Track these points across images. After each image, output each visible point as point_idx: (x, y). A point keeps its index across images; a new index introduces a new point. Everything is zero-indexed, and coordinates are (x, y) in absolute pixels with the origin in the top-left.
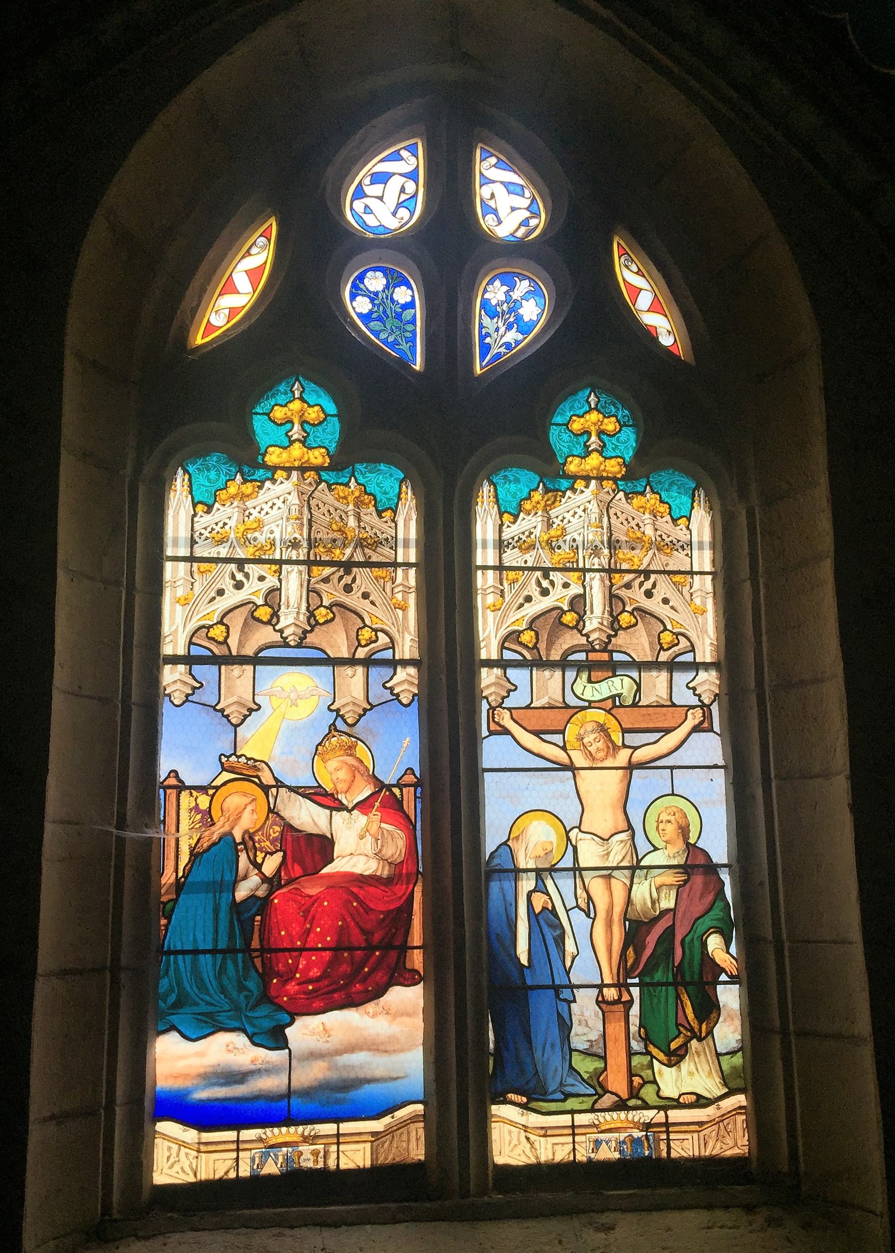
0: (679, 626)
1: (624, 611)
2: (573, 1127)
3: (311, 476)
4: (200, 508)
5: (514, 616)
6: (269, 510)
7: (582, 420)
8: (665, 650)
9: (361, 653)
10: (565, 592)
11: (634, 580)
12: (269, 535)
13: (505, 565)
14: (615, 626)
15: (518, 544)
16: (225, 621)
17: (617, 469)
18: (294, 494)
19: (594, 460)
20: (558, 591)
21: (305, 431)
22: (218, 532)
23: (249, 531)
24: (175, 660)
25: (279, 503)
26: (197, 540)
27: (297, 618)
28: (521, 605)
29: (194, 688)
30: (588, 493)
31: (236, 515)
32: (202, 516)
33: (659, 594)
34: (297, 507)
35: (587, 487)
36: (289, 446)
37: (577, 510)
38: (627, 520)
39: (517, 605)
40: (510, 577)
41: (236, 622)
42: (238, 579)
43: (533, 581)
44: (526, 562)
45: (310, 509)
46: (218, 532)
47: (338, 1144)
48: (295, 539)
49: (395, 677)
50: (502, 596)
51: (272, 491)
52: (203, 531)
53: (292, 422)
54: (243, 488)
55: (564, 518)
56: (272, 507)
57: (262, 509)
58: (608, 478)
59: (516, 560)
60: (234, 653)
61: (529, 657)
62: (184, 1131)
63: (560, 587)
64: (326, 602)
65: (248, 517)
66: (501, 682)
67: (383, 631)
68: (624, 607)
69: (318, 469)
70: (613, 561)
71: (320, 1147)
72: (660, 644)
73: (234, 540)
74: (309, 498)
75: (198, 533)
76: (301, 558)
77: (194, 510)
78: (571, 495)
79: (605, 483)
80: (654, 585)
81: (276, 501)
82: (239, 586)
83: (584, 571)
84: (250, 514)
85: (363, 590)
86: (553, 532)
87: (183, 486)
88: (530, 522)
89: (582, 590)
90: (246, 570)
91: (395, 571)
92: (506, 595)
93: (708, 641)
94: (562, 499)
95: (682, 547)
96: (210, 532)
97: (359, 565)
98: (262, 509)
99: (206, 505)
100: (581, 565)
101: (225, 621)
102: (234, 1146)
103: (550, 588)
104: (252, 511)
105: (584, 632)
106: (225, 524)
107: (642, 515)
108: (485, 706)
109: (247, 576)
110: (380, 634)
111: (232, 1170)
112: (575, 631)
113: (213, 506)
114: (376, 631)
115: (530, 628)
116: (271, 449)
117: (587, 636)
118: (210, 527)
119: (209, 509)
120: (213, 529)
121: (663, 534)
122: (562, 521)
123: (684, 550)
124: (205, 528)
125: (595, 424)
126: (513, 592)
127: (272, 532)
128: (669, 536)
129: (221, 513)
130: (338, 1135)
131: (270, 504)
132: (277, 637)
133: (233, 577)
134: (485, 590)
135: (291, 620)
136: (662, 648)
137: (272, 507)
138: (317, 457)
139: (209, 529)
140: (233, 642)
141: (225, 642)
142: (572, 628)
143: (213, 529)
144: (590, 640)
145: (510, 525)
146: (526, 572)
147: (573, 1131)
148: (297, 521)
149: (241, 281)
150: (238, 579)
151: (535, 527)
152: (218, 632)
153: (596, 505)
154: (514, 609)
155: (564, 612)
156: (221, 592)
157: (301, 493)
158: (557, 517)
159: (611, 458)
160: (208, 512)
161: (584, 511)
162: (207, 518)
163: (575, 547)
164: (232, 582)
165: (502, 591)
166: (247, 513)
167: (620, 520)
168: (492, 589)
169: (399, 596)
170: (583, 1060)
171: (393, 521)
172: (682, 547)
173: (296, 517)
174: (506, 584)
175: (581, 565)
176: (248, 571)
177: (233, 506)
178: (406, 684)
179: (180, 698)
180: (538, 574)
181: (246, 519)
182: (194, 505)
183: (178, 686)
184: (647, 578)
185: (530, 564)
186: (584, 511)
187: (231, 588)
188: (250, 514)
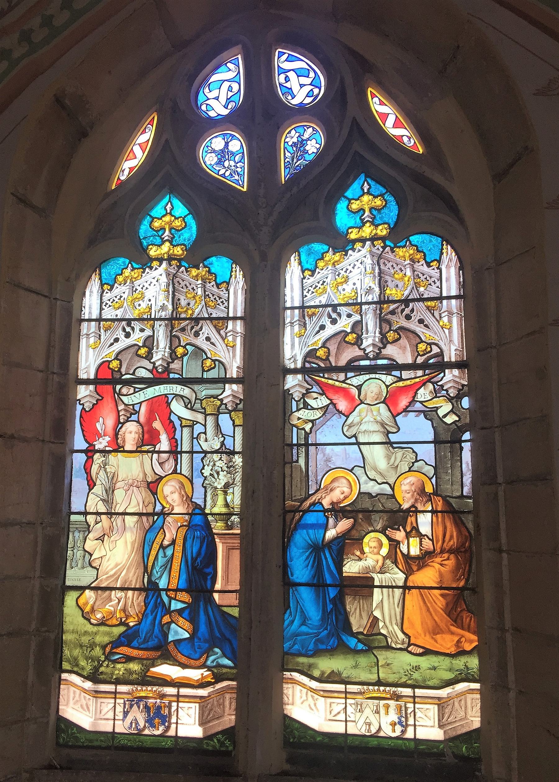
0: (111, 354)
1: (390, 330)
2: (414, 697)
3: (379, 244)
4: (307, 273)
5: (107, 351)
6: (352, 270)
7: (358, 202)
8: (422, 356)
9: (420, 360)
10: (142, 334)
11: (397, 308)
12: (148, 302)
13: (103, 318)
14: (384, 341)
15: (315, 290)
16: (328, 345)
17: (181, 252)
18: (164, 275)
19: (166, 247)
20: (344, 320)
21: (372, 214)
22: (117, 302)
23: (339, 285)
24: (87, 382)
25: (358, 264)
26: (104, 307)
27: (374, 340)
28: (112, 344)
29: (307, 390)
30: (364, 251)
31: (127, 291)
32: (309, 279)
33: (416, 317)
34: (370, 266)
35: (363, 247)
36: (161, 245)
37: (356, 263)
38: (392, 266)
39: (109, 343)
40: (310, 313)
41: (333, 347)
42: (127, 331)
43: (120, 329)
44: (117, 315)
45: (173, 284)
46: (117, 302)
47: (414, 703)
48: (370, 287)
49: (444, 378)
50: (100, 339)
51: (353, 256)
52: (108, 302)
53: (165, 229)
54: (133, 273)
55: (347, 269)
56: (150, 285)
57: (144, 286)
58: (175, 259)
59: (111, 314)
60: (333, 364)
61: (323, 365)
62: (310, 681)
63: (138, 331)
64: (395, 327)
65: (135, 291)
66: (303, 384)
67: (437, 345)
68: (390, 328)
69: (383, 239)
70: (382, 295)
71: (403, 704)
72: (418, 352)
73: (126, 307)
74: (173, 278)
75: (104, 304)
76: (375, 300)
77: (303, 275)
78: (149, 271)
79: (375, 243)
80: (412, 311)
81: (356, 263)
82: (334, 322)
83: (361, 304)
84: (136, 290)
85: (418, 318)
86: (135, 295)
87: (295, 260)
88: (324, 274)
89: (360, 317)
90: (132, 325)
91: (441, 303)
92: (308, 326)
93: (453, 348)
94: (143, 274)
95: (434, 282)
96: (112, 302)
97: (414, 300)
98: (144, 286)
99: (310, 270)
100: (153, 317)
101: (328, 345)
102: (344, 695)
103: (131, 332)
104: (138, 287)
105: (362, 347)
106: (121, 297)
107: (404, 262)
108: (79, 408)
109: (339, 315)
110: (434, 347)
111: (342, 712)
112: (356, 346)
113: (315, 270)
114: (430, 344)
115: (116, 358)
116: (350, 231)
117: (364, 350)
118: (112, 299)
119: (313, 272)
120: (114, 300)
121: (419, 274)
122: (346, 272)
123: (435, 283)
124: (109, 300)
125: (168, 223)
126: (107, 335)
127: (354, 284)
128: (423, 275)
129: (118, 290)
130: (414, 697)
131: (352, 265)
132: (361, 353)
133: (124, 329)
134: (293, 323)
135: (370, 341)
136: (419, 355)
137: (150, 285)
138: (382, 231)
139: (111, 300)
140: (332, 359)
141: (327, 359)
142: (353, 344)
143: (114, 300)
144: (366, 352)
145: (309, 277)
146: (116, 322)
147: (414, 700)
148: (371, 275)
149: (137, 150)
150: (127, 331)
151: (124, 293)
152: (115, 364)
153: (369, 259)
154: (312, 336)
155: (140, 347)
156: (117, 340)
157: (168, 274)
158: (342, 269)
159: (178, 245)
160: (312, 275)
161: (361, 263)
162: (312, 279)
163: (355, 289)
164: (124, 333)
165: (100, 336)
166: (337, 273)
167: (387, 267)
168: (93, 334)
169: (445, 319)
170: (66, 622)
171: (438, 268)
172: (434, 282)
173: (164, 290)
174: (102, 331)
175: (359, 301)
176: (134, 326)
177: (328, 270)
178: (452, 383)
179: (298, 396)
180: (330, 309)
181: (337, 277)
182: (303, 272)
183: (297, 388)
184: (407, 306)
185: (119, 317)
186: (361, 263)
187: (329, 323)
188: (136, 290)
